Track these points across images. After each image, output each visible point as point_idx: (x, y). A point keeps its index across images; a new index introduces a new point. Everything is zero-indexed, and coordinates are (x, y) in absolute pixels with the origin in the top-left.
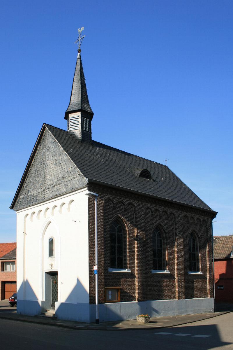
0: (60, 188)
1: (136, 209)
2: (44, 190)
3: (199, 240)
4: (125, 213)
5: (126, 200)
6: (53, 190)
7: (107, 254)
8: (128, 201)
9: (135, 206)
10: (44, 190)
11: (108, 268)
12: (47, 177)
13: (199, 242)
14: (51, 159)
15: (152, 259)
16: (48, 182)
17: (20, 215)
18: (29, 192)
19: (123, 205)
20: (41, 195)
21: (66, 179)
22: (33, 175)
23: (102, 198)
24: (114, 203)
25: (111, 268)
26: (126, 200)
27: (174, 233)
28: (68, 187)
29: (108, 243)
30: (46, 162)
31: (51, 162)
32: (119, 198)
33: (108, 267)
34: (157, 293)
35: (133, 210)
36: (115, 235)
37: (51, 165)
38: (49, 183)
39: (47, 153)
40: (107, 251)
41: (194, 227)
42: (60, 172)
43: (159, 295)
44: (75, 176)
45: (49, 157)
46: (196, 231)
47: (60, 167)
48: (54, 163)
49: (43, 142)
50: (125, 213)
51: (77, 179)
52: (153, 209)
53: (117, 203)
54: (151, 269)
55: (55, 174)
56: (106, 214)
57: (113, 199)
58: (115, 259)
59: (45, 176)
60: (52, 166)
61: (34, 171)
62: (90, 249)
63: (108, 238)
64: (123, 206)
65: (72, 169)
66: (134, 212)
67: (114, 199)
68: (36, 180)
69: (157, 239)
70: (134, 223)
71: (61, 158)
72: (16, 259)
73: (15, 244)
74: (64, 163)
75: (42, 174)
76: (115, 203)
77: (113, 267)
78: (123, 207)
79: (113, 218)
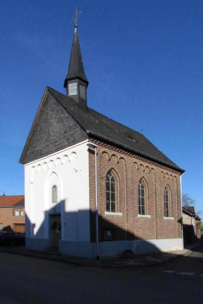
0: (62, 141)
1: (126, 162)
2: (48, 145)
3: (171, 192)
4: (117, 165)
5: (119, 154)
6: (56, 144)
7: (104, 199)
8: (120, 156)
9: (126, 160)
10: (48, 145)
11: (104, 211)
12: (51, 134)
13: (171, 194)
14: (54, 117)
15: (138, 206)
16: (52, 138)
17: (29, 168)
18: (35, 147)
19: (116, 159)
20: (45, 149)
21: (68, 134)
22: (38, 133)
23: (100, 150)
24: (109, 156)
25: (107, 211)
26: (119, 154)
27: (154, 185)
28: (70, 140)
29: (104, 190)
30: (50, 120)
31: (54, 120)
32: (113, 152)
33: (105, 210)
34: (142, 234)
35: (124, 164)
36: (109, 184)
37: (54, 123)
38: (53, 138)
39: (50, 112)
40: (104, 196)
41: (168, 182)
42: (62, 128)
43: (143, 236)
44: (76, 130)
45: (52, 116)
46: (169, 184)
47: (62, 124)
48: (57, 121)
49: (47, 104)
50: (117, 165)
51: (78, 132)
52: (139, 164)
53: (112, 156)
54: (137, 213)
55: (58, 130)
56: (103, 165)
57: (109, 152)
58: (110, 204)
59: (49, 133)
60: (55, 124)
61: (39, 130)
62: (90, 194)
63: (105, 185)
64: (116, 159)
65: (73, 124)
66: (125, 166)
67: (109, 152)
68: (41, 137)
69: (110, 200)
70: (124, 174)
71: (63, 116)
72: (24, 207)
73: (23, 196)
74: (66, 120)
75: (46, 131)
76: (110, 155)
77: (108, 211)
78: (116, 160)
79: (109, 169)
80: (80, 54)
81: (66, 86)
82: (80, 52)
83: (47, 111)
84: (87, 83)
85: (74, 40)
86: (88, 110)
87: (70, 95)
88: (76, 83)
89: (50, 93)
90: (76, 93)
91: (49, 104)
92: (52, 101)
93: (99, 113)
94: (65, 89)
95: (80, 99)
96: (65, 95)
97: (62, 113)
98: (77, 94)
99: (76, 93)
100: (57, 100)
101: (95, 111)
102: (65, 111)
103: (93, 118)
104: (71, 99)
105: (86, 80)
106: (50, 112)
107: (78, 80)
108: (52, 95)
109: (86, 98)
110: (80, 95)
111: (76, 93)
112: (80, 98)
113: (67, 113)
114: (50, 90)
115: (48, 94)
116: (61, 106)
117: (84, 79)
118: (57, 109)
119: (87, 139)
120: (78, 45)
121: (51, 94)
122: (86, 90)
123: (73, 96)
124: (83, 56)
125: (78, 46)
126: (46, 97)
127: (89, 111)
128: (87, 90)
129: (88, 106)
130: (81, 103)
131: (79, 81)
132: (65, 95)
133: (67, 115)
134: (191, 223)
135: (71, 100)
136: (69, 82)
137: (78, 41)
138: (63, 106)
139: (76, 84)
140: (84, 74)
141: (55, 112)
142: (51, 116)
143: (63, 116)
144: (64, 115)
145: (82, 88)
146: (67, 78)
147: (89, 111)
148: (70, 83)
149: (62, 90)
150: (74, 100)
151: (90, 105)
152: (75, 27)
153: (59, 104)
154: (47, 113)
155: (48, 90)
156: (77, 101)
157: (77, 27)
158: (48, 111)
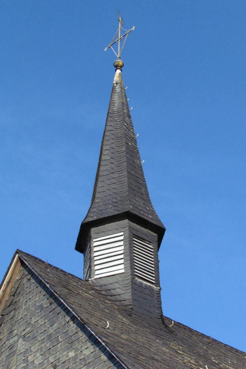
39: (21, 345)
49: (12, 313)
71: (72, 354)
80: (134, 140)
81: (83, 244)
82: (133, 136)
83: (11, 341)
84: (160, 231)
85: (111, 103)
86: (167, 329)
87: (96, 277)
88: (122, 233)
89: (26, 273)
90: (120, 269)
91: (21, 313)
92: (34, 298)
93: (208, 338)
94: (82, 255)
95: (136, 288)
96: (81, 276)
97: (71, 344)
98: (123, 271)
99: (120, 269)
100: (52, 295)
101: (191, 330)
102: (82, 336)
103: (187, 359)
104: (102, 292)
105: (154, 222)
106: (21, 345)
107: (126, 222)
108: (33, 281)
109: (157, 284)
110: (134, 275)
111: (122, 266)
112: (134, 283)
113: (89, 344)
114: (25, 261)
115: (18, 278)
116: (68, 318)
117: (149, 218)
118: (51, 331)
119: (156, 233)
120: (126, 115)
121: (29, 277)
122: (156, 256)
123: (110, 280)
124: (142, 148)
125: (127, 119)
126: (8, 291)
127: (171, 332)
128: (159, 253)
129: (165, 314)
130: (143, 303)
131: (131, 229)
132: (79, 279)
133: (89, 349)
134: (129, 276)
135: (103, 292)
136: (93, 230)
137: (125, 105)
138: (73, 318)
139: (120, 236)
140: (148, 201)
141: (43, 341)
142: (25, 360)
143: (72, 354)
144: (76, 350)
145: (144, 250)
146: (90, 219)
147: (171, 332)
148: (99, 234)
149: (73, 263)
150: (113, 292)
151: (171, 310)
152: (117, 67)
153: (59, 309)
154: (11, 347)
155: (19, 264)
156: (126, 295)
157: (121, 67)
158: (16, 338)
